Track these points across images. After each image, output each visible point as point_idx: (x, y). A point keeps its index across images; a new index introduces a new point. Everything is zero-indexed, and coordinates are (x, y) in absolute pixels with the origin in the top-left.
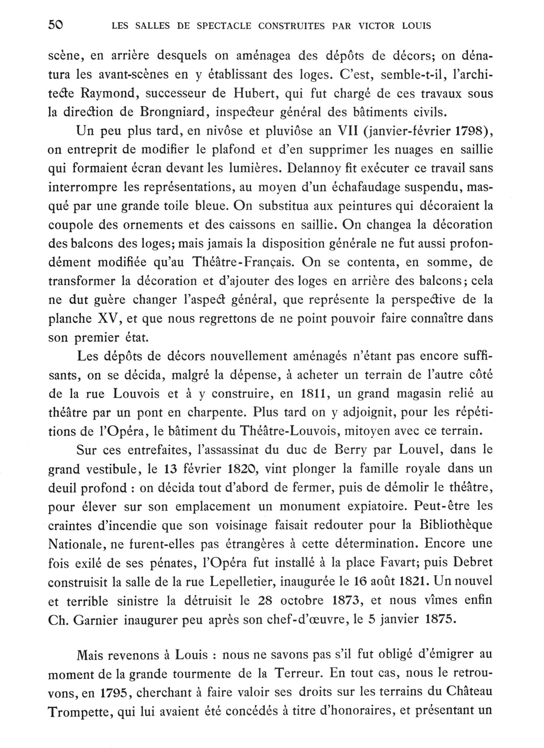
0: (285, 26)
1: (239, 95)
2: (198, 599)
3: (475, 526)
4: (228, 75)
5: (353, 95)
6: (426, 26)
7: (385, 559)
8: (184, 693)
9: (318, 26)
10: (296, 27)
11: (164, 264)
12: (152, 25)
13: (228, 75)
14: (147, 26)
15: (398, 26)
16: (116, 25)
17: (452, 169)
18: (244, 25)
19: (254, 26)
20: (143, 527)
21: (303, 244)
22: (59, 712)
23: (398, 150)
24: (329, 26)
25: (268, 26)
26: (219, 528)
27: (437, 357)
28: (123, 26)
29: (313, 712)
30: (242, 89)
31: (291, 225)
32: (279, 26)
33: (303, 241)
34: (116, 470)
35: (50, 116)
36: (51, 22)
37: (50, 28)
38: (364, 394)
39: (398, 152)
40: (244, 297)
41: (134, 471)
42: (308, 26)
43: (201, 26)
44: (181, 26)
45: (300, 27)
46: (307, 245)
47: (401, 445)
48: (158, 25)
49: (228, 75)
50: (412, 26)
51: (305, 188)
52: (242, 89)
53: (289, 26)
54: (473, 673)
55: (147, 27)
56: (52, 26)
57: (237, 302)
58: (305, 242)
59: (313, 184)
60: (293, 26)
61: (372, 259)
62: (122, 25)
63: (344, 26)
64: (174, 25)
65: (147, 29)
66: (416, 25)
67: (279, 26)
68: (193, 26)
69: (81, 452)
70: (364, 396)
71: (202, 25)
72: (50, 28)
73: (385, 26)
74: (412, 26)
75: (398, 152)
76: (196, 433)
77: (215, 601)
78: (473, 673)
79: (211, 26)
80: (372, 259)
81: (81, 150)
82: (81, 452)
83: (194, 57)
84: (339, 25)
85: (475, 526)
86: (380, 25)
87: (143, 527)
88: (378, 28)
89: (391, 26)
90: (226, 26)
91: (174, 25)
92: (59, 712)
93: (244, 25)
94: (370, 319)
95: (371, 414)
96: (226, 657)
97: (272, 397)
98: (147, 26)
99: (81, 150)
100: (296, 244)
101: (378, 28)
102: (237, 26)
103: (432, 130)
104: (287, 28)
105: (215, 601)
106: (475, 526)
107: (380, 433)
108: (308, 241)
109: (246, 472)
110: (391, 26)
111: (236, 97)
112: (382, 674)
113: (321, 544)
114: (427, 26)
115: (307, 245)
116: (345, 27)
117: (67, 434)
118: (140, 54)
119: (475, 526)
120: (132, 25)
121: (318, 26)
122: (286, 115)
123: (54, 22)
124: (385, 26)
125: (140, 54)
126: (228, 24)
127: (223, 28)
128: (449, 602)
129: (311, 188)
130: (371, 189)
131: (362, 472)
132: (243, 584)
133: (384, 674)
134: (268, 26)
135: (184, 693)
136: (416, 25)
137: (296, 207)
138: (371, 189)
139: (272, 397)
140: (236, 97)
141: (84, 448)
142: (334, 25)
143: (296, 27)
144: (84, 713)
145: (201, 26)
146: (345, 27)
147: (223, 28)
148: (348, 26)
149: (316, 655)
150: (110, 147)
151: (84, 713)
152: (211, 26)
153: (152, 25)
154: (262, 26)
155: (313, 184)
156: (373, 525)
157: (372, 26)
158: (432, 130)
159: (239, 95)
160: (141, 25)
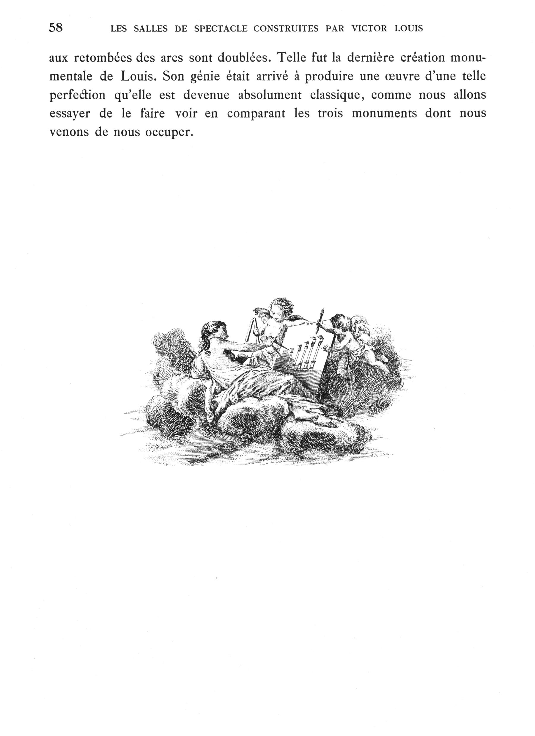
0: (279, 28)
4: (243, 59)
6: (418, 28)
8: (278, 113)
10: (291, 29)
12: (150, 28)
13: (242, 58)
16: (115, 28)
18: (241, 28)
24: (322, 28)
26: (53, 134)
28: (313, 29)
32: (274, 29)
35: (334, 61)
36: (51, 25)
37: (50, 31)
41: (357, 96)
42: (302, 28)
43: (199, 29)
44: (178, 29)
45: (295, 29)
48: (156, 28)
49: (242, 58)
50: (404, 28)
51: (428, 77)
54: (326, 114)
55: (145, 30)
56: (52, 29)
57: (196, 79)
60: (288, 29)
62: (121, 28)
63: (338, 29)
64: (171, 28)
65: (146, 32)
66: (408, 28)
67: (274, 29)
68: (190, 29)
71: (199, 28)
72: (50, 31)
73: (377, 28)
74: (404, 28)
78: (326, 114)
79: (208, 28)
84: (332, 27)
86: (372, 28)
88: (371, 31)
89: (384, 28)
90: (223, 29)
91: (171, 28)
93: (241, 28)
94: (192, 114)
96: (422, 97)
97: (363, 98)
101: (371, 31)
103: (410, 75)
114: (419, 28)
116: (338, 29)
122: (196, 79)
124: (377, 28)
127: (220, 31)
128: (301, 115)
129: (434, 77)
130: (220, 97)
132: (476, 78)
135: (278, 113)
136: (408, 28)
138: (220, 97)
139: (363, 98)
142: (328, 28)
143: (291, 29)
145: (199, 29)
146: (338, 29)
147: (220, 31)
148: (341, 28)
150: (273, 73)
151: (254, 114)
152: (208, 28)
153: (150, 28)
154: (257, 28)
157: (365, 28)
158: (410, 75)
160: (139, 28)
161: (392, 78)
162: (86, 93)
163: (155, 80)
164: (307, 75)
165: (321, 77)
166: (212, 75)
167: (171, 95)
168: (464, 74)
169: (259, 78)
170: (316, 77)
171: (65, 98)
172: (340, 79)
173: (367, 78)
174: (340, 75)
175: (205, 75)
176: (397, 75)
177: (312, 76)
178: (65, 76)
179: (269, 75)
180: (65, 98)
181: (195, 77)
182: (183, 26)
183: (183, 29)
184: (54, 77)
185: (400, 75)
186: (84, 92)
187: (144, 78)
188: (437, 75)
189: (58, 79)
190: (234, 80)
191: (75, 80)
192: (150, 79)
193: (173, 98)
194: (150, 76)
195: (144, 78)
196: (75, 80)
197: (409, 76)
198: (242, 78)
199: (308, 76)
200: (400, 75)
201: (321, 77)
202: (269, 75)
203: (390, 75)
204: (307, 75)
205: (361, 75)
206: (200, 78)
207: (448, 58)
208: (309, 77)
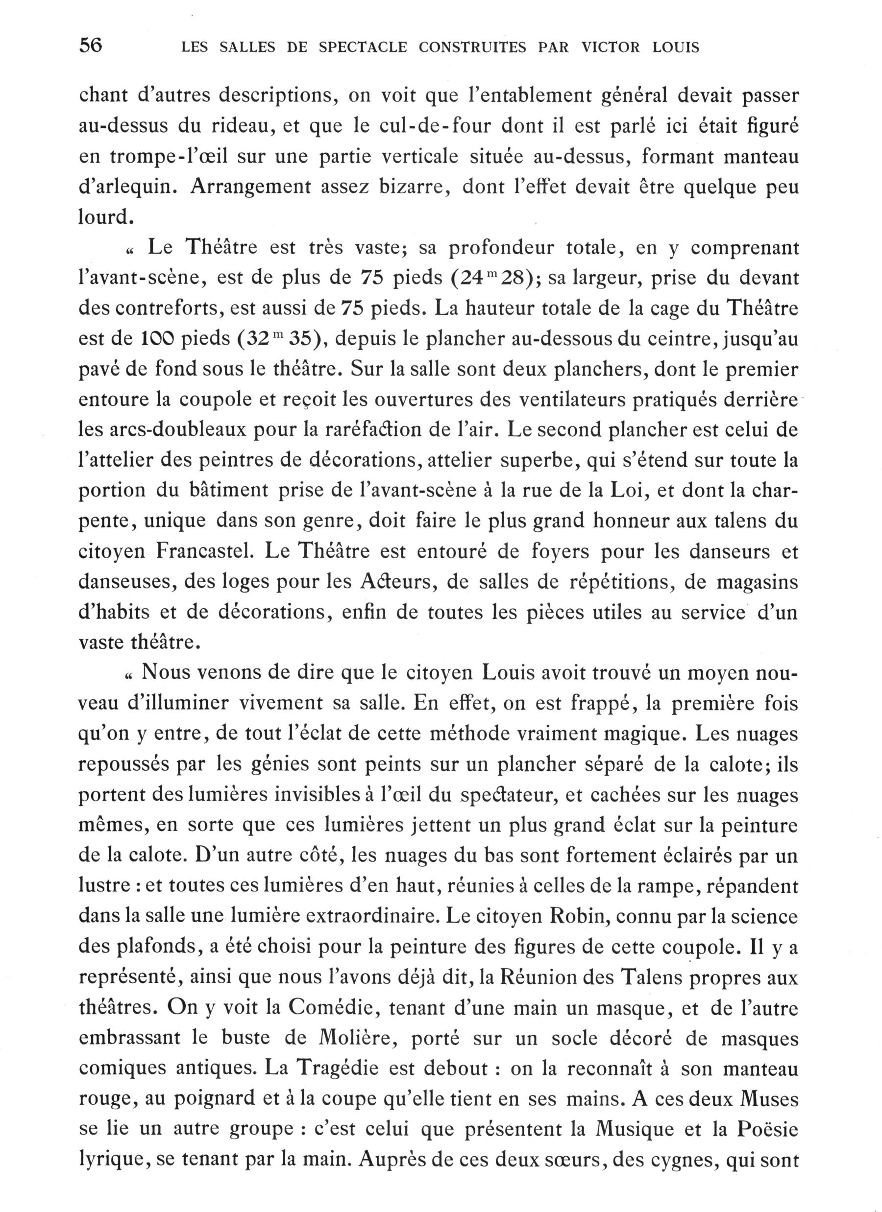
0: (462, 47)
3: (136, 188)
5: (588, 280)
6: (691, 48)
9: (516, 47)
10: (480, 48)
11: (767, 342)
12: (246, 46)
14: (238, 48)
15: (646, 47)
16: (189, 46)
17: (390, 492)
18: (396, 47)
19: (412, 47)
21: (485, 157)
23: (391, 855)
25: (435, 47)
29: (329, 675)
32: (452, 48)
36: (84, 41)
38: (564, 825)
39: (391, 858)
43: (326, 47)
44: (293, 48)
45: (487, 49)
47: (438, 300)
48: (256, 46)
50: (668, 47)
53: (469, 47)
55: (239, 49)
60: (475, 48)
61: (523, 791)
62: (198, 47)
63: (558, 48)
66: (674, 46)
67: (452, 48)
68: (313, 47)
70: (563, 829)
73: (624, 47)
74: (668, 47)
75: (391, 858)
76: (562, 737)
77: (381, 339)
80: (523, 791)
84: (549, 45)
85: (136, 189)
86: (616, 46)
88: (613, 51)
89: (634, 47)
90: (366, 47)
95: (203, 1101)
98: (238, 48)
101: (613, 51)
102: (383, 47)
104: (465, 51)
105: (381, 339)
106: (136, 188)
107: (129, 554)
109: (510, 283)
110: (634, 47)
112: (715, 766)
114: (692, 47)
116: (558, 49)
118: (783, 398)
119: (136, 189)
120: (214, 46)
121: (516, 47)
123: (89, 41)
124: (624, 47)
125: (783, 398)
126: (369, 44)
127: (362, 51)
131: (419, 526)
133: (719, 766)
134: (435, 47)
136: (674, 46)
137: (491, 158)
142: (541, 46)
143: (480, 48)
145: (326, 47)
146: (558, 49)
147: (362, 51)
148: (564, 47)
153: (246, 46)
154: (425, 47)
157: (603, 47)
160: (229, 46)
175: (275, 762)
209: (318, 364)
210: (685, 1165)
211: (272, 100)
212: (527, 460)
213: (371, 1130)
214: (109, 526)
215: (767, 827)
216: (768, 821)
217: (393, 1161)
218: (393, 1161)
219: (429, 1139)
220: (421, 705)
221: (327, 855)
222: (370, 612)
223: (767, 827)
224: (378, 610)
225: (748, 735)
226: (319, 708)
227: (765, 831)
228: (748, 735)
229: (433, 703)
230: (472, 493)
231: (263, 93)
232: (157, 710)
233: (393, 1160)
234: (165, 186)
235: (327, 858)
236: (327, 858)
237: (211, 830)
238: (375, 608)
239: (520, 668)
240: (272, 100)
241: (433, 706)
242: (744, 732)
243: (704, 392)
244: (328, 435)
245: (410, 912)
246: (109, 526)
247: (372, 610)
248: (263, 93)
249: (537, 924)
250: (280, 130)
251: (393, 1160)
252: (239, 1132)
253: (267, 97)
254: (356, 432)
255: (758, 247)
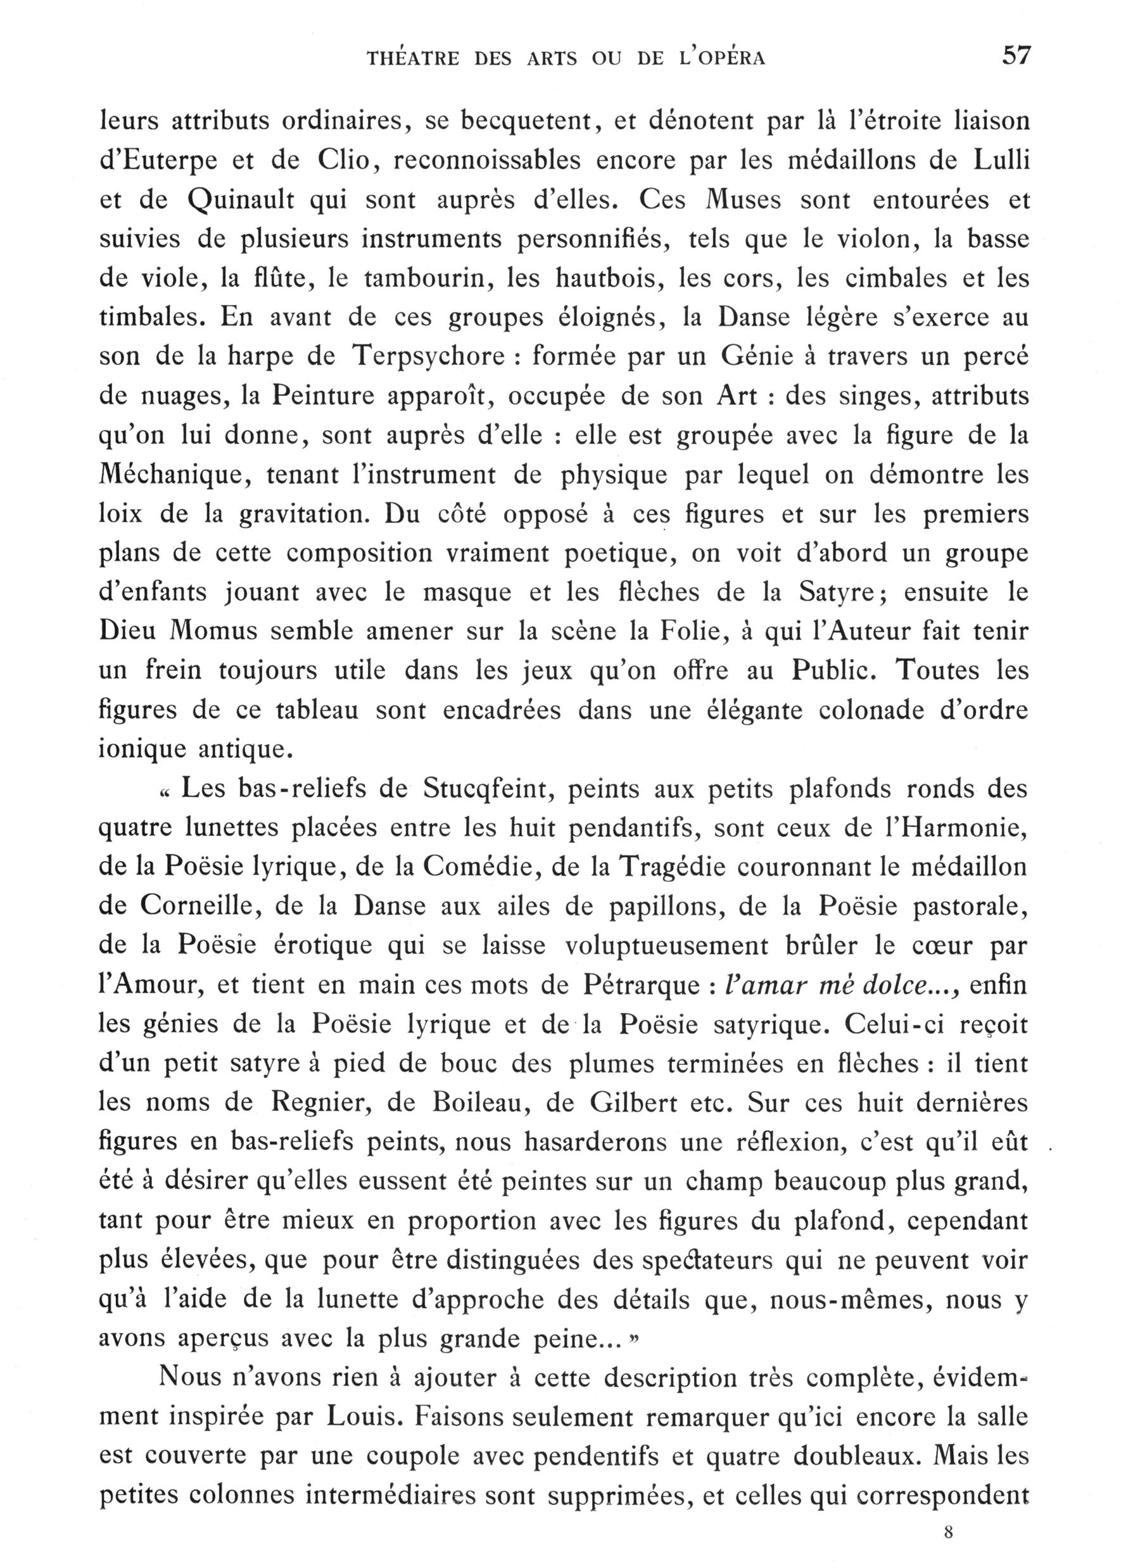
1: (912, 831)
2: (470, 1176)
7: (423, 1410)
10: (447, 60)
20: (503, 712)
21: (387, 554)
22: (644, 865)
27: (631, 162)
30: (919, 818)
31: (254, 712)
33: (386, 548)
34: (228, 122)
40: (169, 1018)
44: (645, 60)
46: (395, 555)
52: (919, 818)
53: (432, 58)
57: (156, 1029)
58: (391, 550)
59: (122, 1056)
60: (439, 60)
63: (540, 59)
69: (756, 1106)
81: (655, 829)
82: (758, 1107)
83: (795, 478)
87: (503, 712)
92: (644, 865)
95: (602, 321)
99: (655, 829)
100: (373, 555)
103: (280, 1061)
108: (396, 547)
111: (906, 834)
113: (558, 673)
115: (395, 555)
116: (540, 60)
117: (648, 1146)
122: (156, 1029)
129: (117, 1063)
140: (906, 834)
141: (762, 1099)
143: (447, 60)
144: (511, 318)
146: (540, 60)
149: (635, 357)
155: (122, 1056)
156: (576, 789)
158: (280, 1061)
159: (912, 831)
161: (940, 949)
162: (697, 1257)
163: (400, 1423)
164: (993, 943)
165: (496, 1302)
166: (989, 511)
167: (653, 436)
168: (977, 628)
169: (341, 673)
170: (486, 1302)
171: (693, 1071)
172: (609, 246)
173: (658, 1185)
174: (232, 197)
176: (889, 629)
177: (480, 200)
178: (914, 591)
179: (899, 1493)
180: (693, 1071)
181: (193, 397)
182: (655, 53)
183: (655, 59)
184: (1019, 1222)
185: (183, 1452)
186: (693, 1254)
187: (376, 1420)
188: (125, 1060)
189: (397, 638)
190: (647, 1307)
191: (301, 521)
192: (390, 1422)
193: (658, 443)
194: (886, 787)
195: (376, 1420)
196: (301, 521)
197: (459, 553)
198: (358, 124)
199: (415, 1221)
200: (183, 1452)
201: (496, 1302)
202: (899, 1493)
203: (936, 944)
204: (102, 1257)
205: (102, 667)
206: (164, 1027)
207: (743, 1380)
208: (416, 1222)
209: (757, 1451)
210: (321, 1109)
211: (672, 1385)
212: (571, 397)
213: (541, 1380)
214: (478, 246)
215: (335, 397)
216: (336, 390)
217: (472, 201)
218: (472, 201)
219: (480, 605)
220: (230, 320)
221: (472, 515)
222: (1005, 985)
223: (335, 397)
224: (1016, 983)
225: (156, 397)
226: (750, 128)
227: (332, 403)
228: (156, 397)
229: (246, 317)
230: (713, 635)
231: (661, 1376)
232: (1015, 170)
233: (472, 200)
234: (478, 278)
235: (472, 517)
236: (472, 517)
237: (888, 1503)
238: (1012, 980)
239: (126, 233)
240: (672, 1385)
241: (246, 321)
242: (152, 393)
243: (587, 386)
244: (644, 874)
245: (393, 980)
246: (478, 246)
247: (1008, 983)
248: (661, 1376)
249: (211, 1151)
250: (699, 1502)
251: (472, 200)
252: (958, 558)
253: (667, 1381)
254: (754, 1146)
255: (463, 238)
